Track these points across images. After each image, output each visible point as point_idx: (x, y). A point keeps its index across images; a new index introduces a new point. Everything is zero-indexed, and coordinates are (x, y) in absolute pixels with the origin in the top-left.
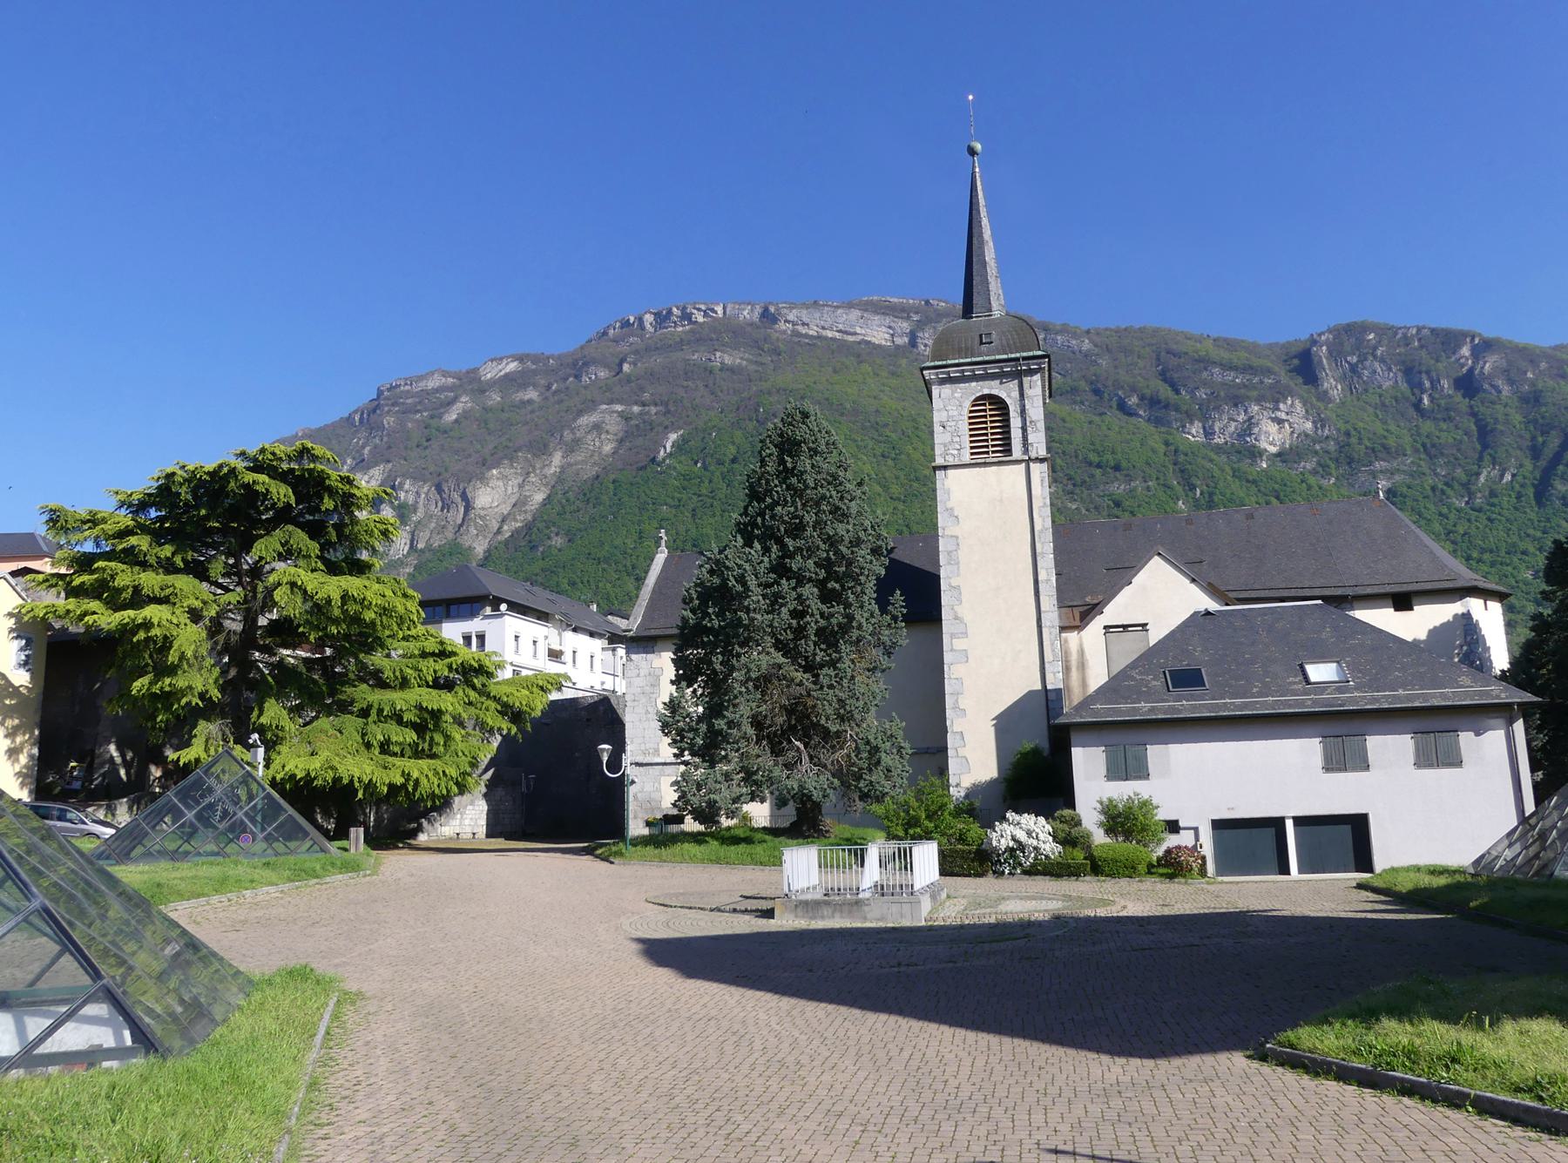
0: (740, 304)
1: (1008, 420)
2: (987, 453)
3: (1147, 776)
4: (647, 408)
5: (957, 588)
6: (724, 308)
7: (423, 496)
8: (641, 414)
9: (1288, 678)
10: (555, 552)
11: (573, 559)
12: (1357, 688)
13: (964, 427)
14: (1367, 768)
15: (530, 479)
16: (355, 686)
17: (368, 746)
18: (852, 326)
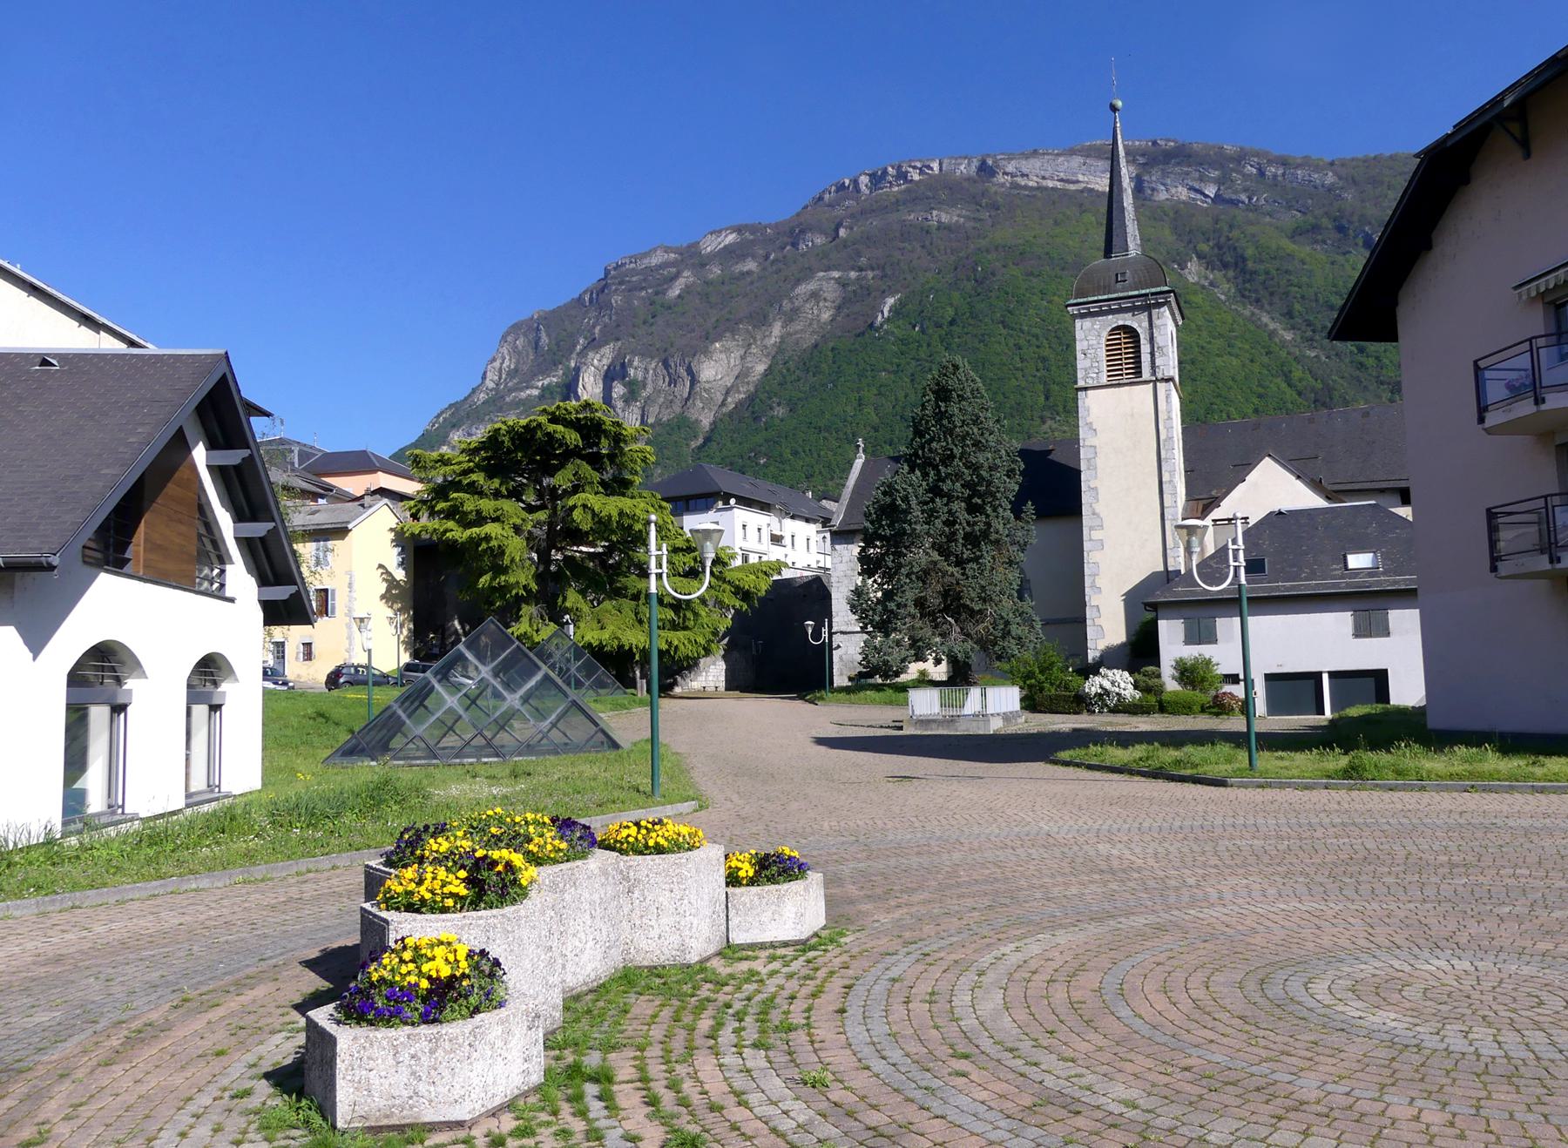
0: (956, 159)
1: (1139, 347)
2: (1122, 375)
3: (1215, 641)
4: (864, 273)
5: (1095, 489)
6: (941, 164)
7: (651, 372)
8: (858, 279)
10: (777, 422)
11: (795, 429)
12: (1384, 573)
13: (1103, 353)
14: (1388, 634)
15: (752, 351)
16: (627, 577)
17: (640, 622)
18: (1074, 174)
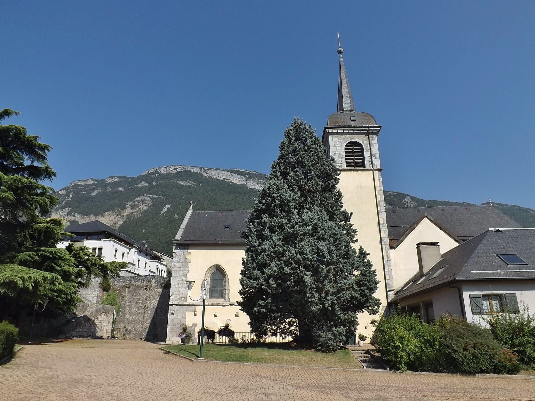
15: (118, 216)
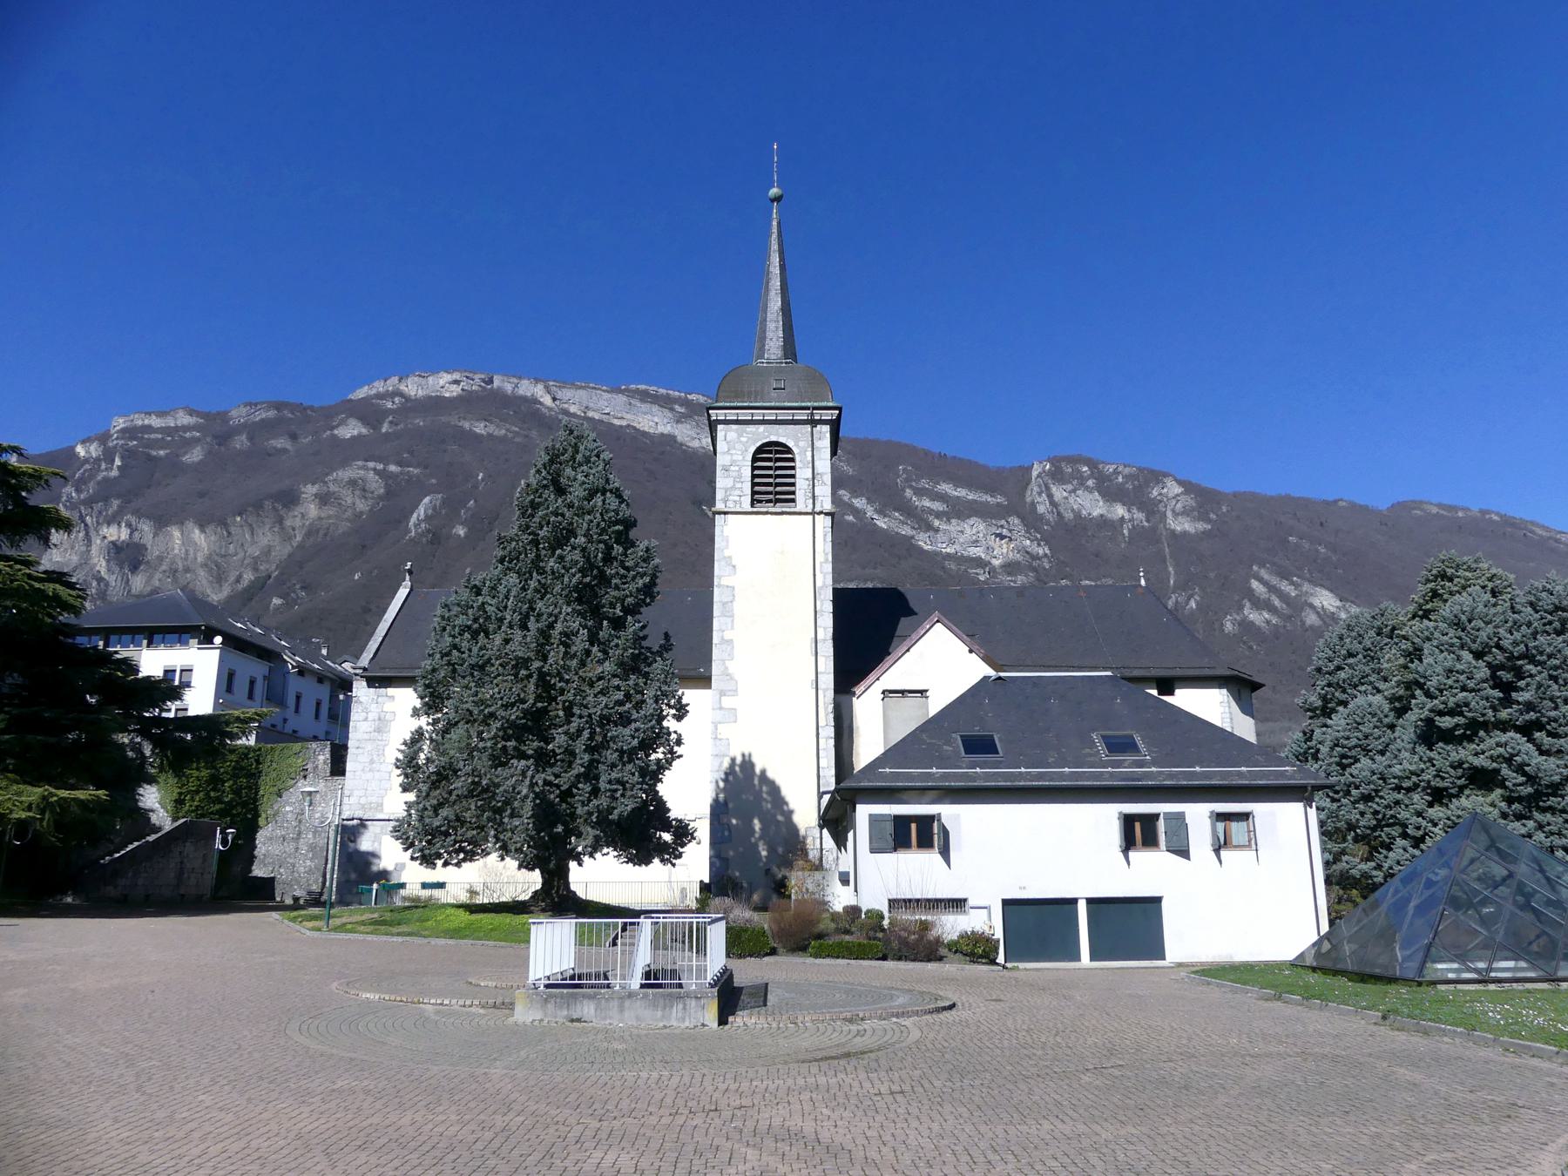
5: (730, 642)
9: (1084, 749)
12: (1154, 763)
